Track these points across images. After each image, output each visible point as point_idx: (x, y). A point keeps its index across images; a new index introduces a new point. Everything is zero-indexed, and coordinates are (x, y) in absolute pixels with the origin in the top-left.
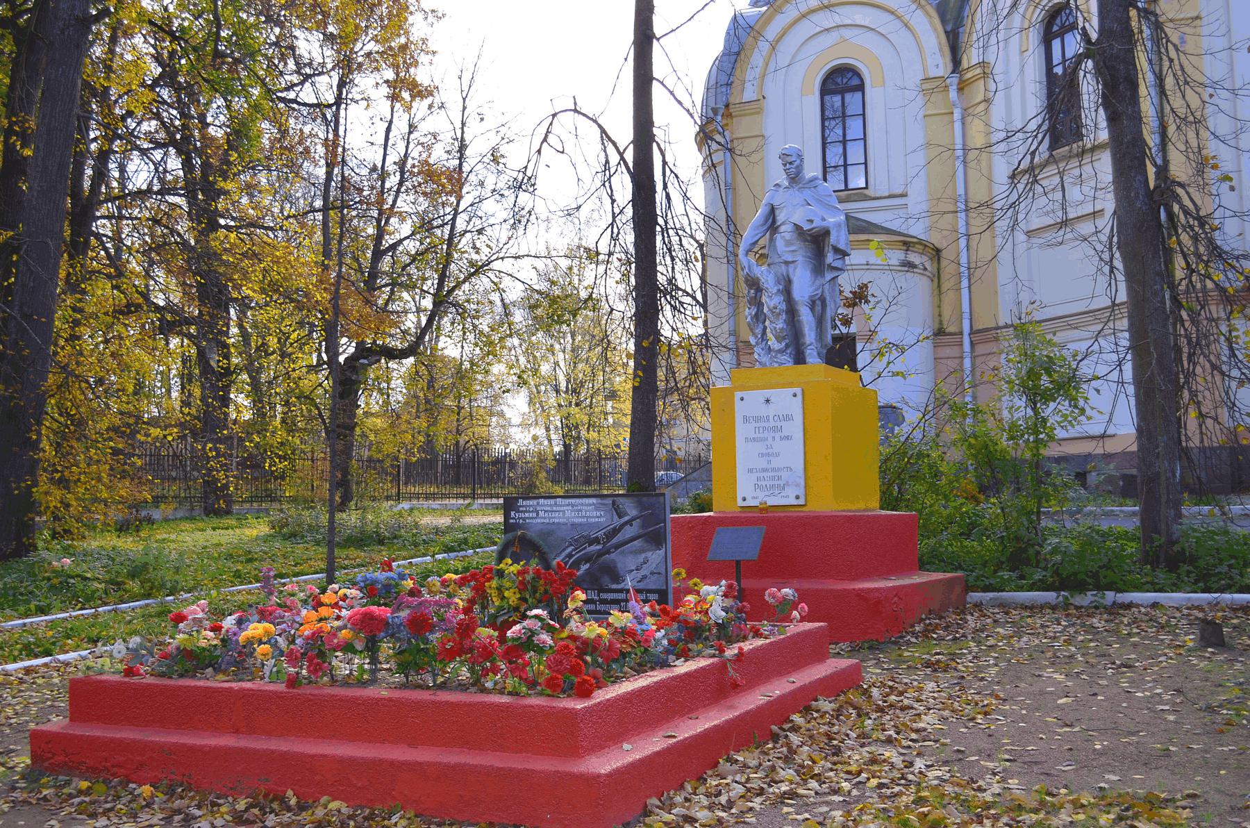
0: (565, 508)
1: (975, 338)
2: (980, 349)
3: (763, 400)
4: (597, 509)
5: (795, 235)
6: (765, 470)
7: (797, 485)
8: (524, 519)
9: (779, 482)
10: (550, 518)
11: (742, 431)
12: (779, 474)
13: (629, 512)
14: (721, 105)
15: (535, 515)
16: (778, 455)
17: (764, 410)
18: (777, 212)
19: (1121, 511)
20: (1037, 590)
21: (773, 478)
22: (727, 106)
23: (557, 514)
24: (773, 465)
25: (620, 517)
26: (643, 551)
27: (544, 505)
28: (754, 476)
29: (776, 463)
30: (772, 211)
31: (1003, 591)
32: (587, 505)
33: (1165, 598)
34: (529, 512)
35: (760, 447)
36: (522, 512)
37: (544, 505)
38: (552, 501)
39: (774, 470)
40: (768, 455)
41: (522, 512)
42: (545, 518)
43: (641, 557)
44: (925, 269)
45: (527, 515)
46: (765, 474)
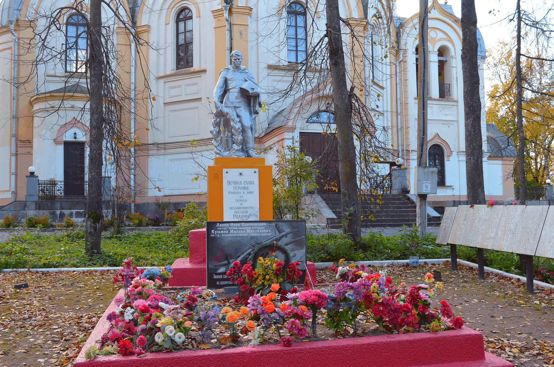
0: (247, 228)
3: (238, 173)
4: (266, 228)
5: (240, 95)
6: (240, 208)
7: (256, 216)
8: (221, 234)
9: (247, 214)
10: (237, 234)
11: (227, 188)
12: (246, 210)
14: (14, 19)
15: (227, 232)
16: (246, 201)
17: (239, 179)
18: (229, 82)
21: (243, 212)
22: (17, 20)
23: (242, 231)
25: (280, 233)
27: (234, 227)
28: (233, 211)
29: (245, 205)
30: (226, 81)
34: (224, 230)
36: (219, 230)
37: (234, 227)
38: (239, 224)
39: (243, 208)
40: (241, 200)
41: (219, 230)
42: (234, 234)
45: (222, 232)
46: (239, 210)
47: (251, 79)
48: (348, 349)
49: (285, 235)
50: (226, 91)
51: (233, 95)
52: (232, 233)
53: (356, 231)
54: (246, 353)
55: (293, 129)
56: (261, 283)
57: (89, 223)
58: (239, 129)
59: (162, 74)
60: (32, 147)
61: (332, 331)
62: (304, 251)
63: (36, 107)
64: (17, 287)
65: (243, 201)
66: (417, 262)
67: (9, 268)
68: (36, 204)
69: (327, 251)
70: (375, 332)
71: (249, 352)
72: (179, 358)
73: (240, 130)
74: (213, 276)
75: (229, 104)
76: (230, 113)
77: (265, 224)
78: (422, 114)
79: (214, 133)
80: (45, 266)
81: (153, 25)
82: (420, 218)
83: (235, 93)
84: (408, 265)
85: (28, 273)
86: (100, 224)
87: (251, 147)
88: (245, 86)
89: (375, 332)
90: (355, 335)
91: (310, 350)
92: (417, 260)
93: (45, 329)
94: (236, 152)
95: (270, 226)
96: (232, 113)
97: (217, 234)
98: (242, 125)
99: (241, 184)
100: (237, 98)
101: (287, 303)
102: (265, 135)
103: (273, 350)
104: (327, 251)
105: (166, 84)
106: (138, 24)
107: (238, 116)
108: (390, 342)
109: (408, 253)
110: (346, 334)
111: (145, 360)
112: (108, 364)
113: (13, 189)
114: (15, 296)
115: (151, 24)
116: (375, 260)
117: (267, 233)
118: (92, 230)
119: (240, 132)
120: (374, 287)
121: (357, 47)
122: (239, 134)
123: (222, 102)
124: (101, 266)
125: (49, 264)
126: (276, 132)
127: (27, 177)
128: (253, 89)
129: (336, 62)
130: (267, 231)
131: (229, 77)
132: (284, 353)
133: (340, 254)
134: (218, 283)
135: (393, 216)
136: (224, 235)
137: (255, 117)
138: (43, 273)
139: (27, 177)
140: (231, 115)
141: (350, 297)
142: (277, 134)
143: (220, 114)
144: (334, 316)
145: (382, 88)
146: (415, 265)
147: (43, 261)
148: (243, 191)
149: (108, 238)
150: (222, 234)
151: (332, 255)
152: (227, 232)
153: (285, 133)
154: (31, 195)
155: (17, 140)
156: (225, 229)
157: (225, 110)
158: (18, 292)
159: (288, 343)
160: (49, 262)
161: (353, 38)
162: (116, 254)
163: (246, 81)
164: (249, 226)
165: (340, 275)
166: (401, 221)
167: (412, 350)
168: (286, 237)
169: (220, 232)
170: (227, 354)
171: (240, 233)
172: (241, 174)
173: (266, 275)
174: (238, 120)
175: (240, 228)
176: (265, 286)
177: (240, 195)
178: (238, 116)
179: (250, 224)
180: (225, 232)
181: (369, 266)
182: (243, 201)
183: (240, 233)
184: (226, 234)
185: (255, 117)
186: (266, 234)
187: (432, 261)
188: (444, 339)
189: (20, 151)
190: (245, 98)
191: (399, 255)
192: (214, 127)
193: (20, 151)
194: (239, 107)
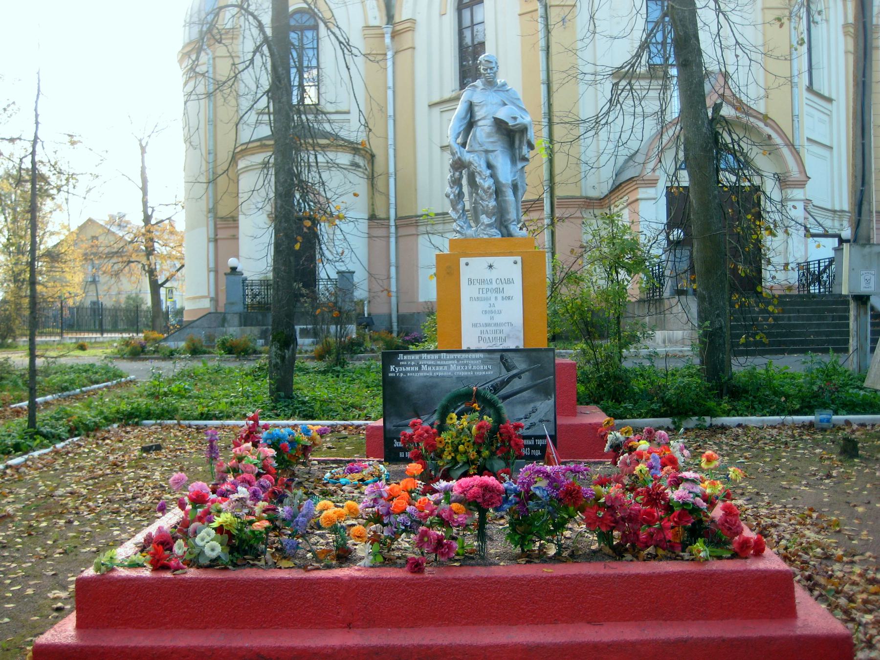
0: (450, 362)
1: (399, 223)
2: (402, 231)
3: (486, 265)
4: (484, 362)
6: (487, 325)
7: (517, 338)
8: (405, 373)
9: (501, 335)
10: (433, 372)
11: (466, 292)
12: (501, 328)
13: (517, 364)
15: (417, 369)
16: (500, 312)
17: (488, 275)
18: (476, 109)
19: (566, 353)
20: (650, 417)
21: (496, 332)
23: (441, 368)
24: (495, 321)
25: (508, 370)
26: (531, 401)
27: (427, 360)
28: (478, 330)
29: (498, 319)
31: (625, 418)
32: (473, 359)
33: (745, 420)
34: (411, 366)
35: (484, 305)
36: (403, 366)
37: (427, 360)
38: (436, 356)
39: (496, 325)
40: (491, 312)
41: (403, 366)
42: (428, 372)
43: (530, 407)
44: (366, 169)
45: (408, 369)
46: (488, 328)
47: (515, 101)
48: (523, 585)
49: (518, 375)
50: (470, 124)
51: (483, 130)
52: (424, 371)
53: (723, 361)
54: (342, 579)
55: (653, 183)
56: (449, 458)
57: (274, 349)
58: (489, 188)
59: (436, 99)
60: (237, 227)
61: (518, 550)
62: (551, 402)
63: (242, 164)
64: (146, 450)
65: (495, 312)
66: (828, 421)
67: (151, 419)
68: (240, 317)
69: (662, 398)
70: (593, 556)
71: (347, 578)
72: (233, 580)
73: (491, 191)
74: (394, 443)
75: (477, 147)
76: (474, 162)
77: (481, 355)
78: (860, 147)
79: (452, 196)
80: (203, 416)
81: (421, 19)
82: (855, 339)
83: (486, 128)
84: (811, 424)
85: (176, 427)
86: (291, 350)
87: (512, 219)
88: (503, 114)
89: (593, 556)
90: (557, 558)
91: (454, 581)
92: (829, 417)
93: (144, 517)
94: (485, 228)
95: (491, 359)
96: (478, 162)
97: (399, 372)
98: (497, 182)
99: (491, 283)
100: (489, 135)
101: (431, 498)
102: (612, 192)
103: (389, 577)
104: (662, 398)
105: (445, 114)
106: (397, 19)
107: (489, 166)
108: (604, 576)
109: (816, 403)
110: (541, 557)
111: (180, 579)
112: (125, 582)
113: (212, 295)
114: (138, 464)
115: (418, 18)
116: (752, 415)
117: (485, 370)
118: (278, 361)
119: (491, 194)
120: (641, 471)
121: (726, 31)
122: (490, 197)
123: (464, 145)
124: (288, 419)
125: (208, 414)
126: (625, 189)
127: (226, 274)
128: (515, 118)
129: (685, 60)
130: (486, 367)
131: (476, 99)
132: (408, 585)
133: (684, 404)
134: (402, 455)
135: (832, 334)
136: (411, 374)
137: (523, 167)
138: (198, 428)
139: (226, 274)
140: (476, 165)
141: (538, 492)
142: (627, 191)
143: (459, 165)
144: (516, 524)
145: (829, 100)
146: (825, 425)
147: (200, 409)
148: (494, 295)
149: (319, 372)
150: (408, 372)
151: (670, 406)
152: (417, 369)
153: (640, 190)
154: (232, 304)
155: (216, 218)
156: (413, 363)
157: (468, 157)
158: (144, 458)
159: (416, 566)
160: (209, 411)
161: (718, 17)
162: (315, 399)
163: (505, 104)
164: (454, 359)
165: (611, 447)
166: (829, 342)
167: (647, 591)
168: (520, 378)
169: (404, 370)
170: (309, 579)
171: (438, 371)
172: (491, 266)
173: (459, 444)
174: (488, 172)
175: (439, 363)
176: (457, 463)
177: (489, 302)
178: (489, 166)
179: (456, 355)
180: (413, 369)
181: (739, 425)
182: (495, 312)
183: (438, 371)
184: (414, 372)
185: (523, 167)
186: (484, 373)
187: (860, 419)
188: (711, 575)
189: (222, 234)
190: (504, 135)
191: (798, 406)
192: (452, 188)
193: (222, 234)
194: (493, 151)
